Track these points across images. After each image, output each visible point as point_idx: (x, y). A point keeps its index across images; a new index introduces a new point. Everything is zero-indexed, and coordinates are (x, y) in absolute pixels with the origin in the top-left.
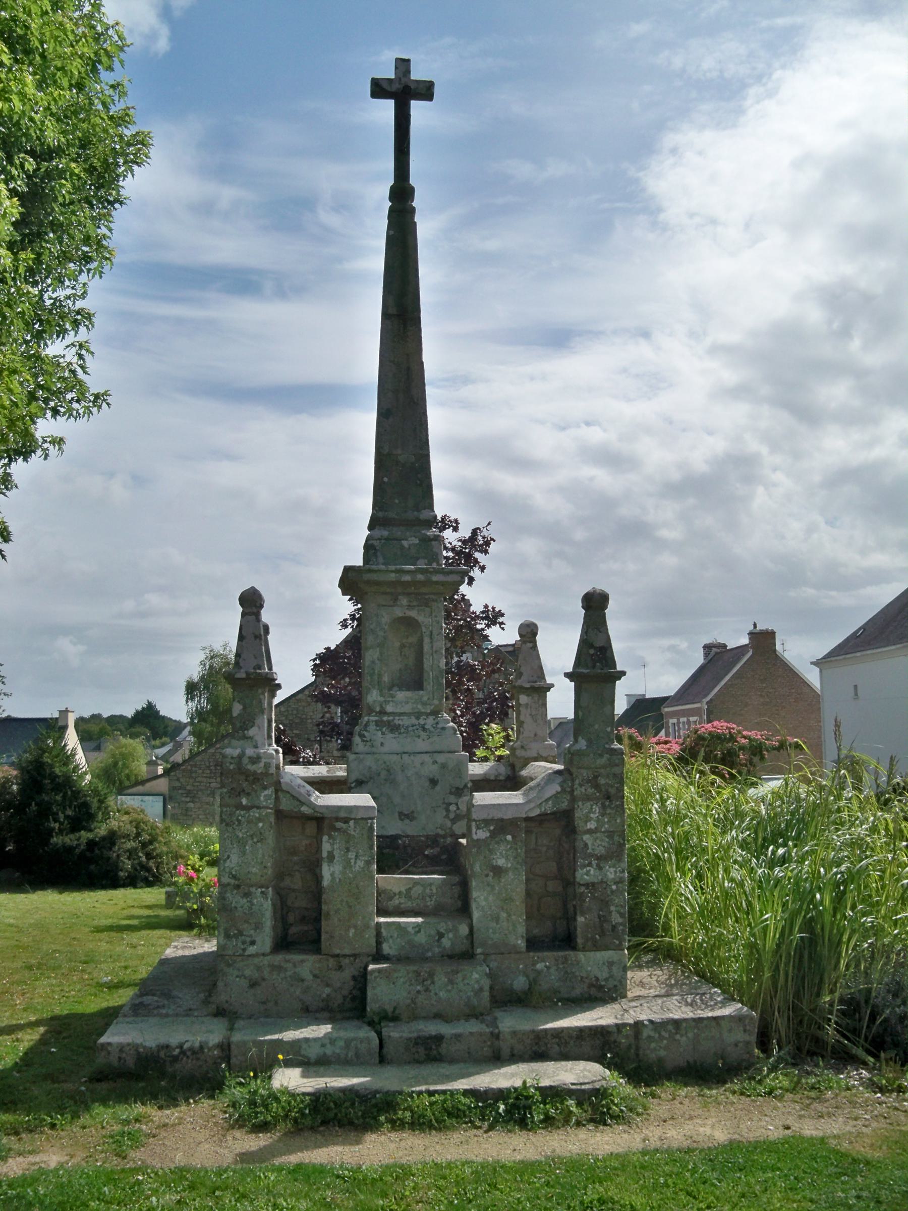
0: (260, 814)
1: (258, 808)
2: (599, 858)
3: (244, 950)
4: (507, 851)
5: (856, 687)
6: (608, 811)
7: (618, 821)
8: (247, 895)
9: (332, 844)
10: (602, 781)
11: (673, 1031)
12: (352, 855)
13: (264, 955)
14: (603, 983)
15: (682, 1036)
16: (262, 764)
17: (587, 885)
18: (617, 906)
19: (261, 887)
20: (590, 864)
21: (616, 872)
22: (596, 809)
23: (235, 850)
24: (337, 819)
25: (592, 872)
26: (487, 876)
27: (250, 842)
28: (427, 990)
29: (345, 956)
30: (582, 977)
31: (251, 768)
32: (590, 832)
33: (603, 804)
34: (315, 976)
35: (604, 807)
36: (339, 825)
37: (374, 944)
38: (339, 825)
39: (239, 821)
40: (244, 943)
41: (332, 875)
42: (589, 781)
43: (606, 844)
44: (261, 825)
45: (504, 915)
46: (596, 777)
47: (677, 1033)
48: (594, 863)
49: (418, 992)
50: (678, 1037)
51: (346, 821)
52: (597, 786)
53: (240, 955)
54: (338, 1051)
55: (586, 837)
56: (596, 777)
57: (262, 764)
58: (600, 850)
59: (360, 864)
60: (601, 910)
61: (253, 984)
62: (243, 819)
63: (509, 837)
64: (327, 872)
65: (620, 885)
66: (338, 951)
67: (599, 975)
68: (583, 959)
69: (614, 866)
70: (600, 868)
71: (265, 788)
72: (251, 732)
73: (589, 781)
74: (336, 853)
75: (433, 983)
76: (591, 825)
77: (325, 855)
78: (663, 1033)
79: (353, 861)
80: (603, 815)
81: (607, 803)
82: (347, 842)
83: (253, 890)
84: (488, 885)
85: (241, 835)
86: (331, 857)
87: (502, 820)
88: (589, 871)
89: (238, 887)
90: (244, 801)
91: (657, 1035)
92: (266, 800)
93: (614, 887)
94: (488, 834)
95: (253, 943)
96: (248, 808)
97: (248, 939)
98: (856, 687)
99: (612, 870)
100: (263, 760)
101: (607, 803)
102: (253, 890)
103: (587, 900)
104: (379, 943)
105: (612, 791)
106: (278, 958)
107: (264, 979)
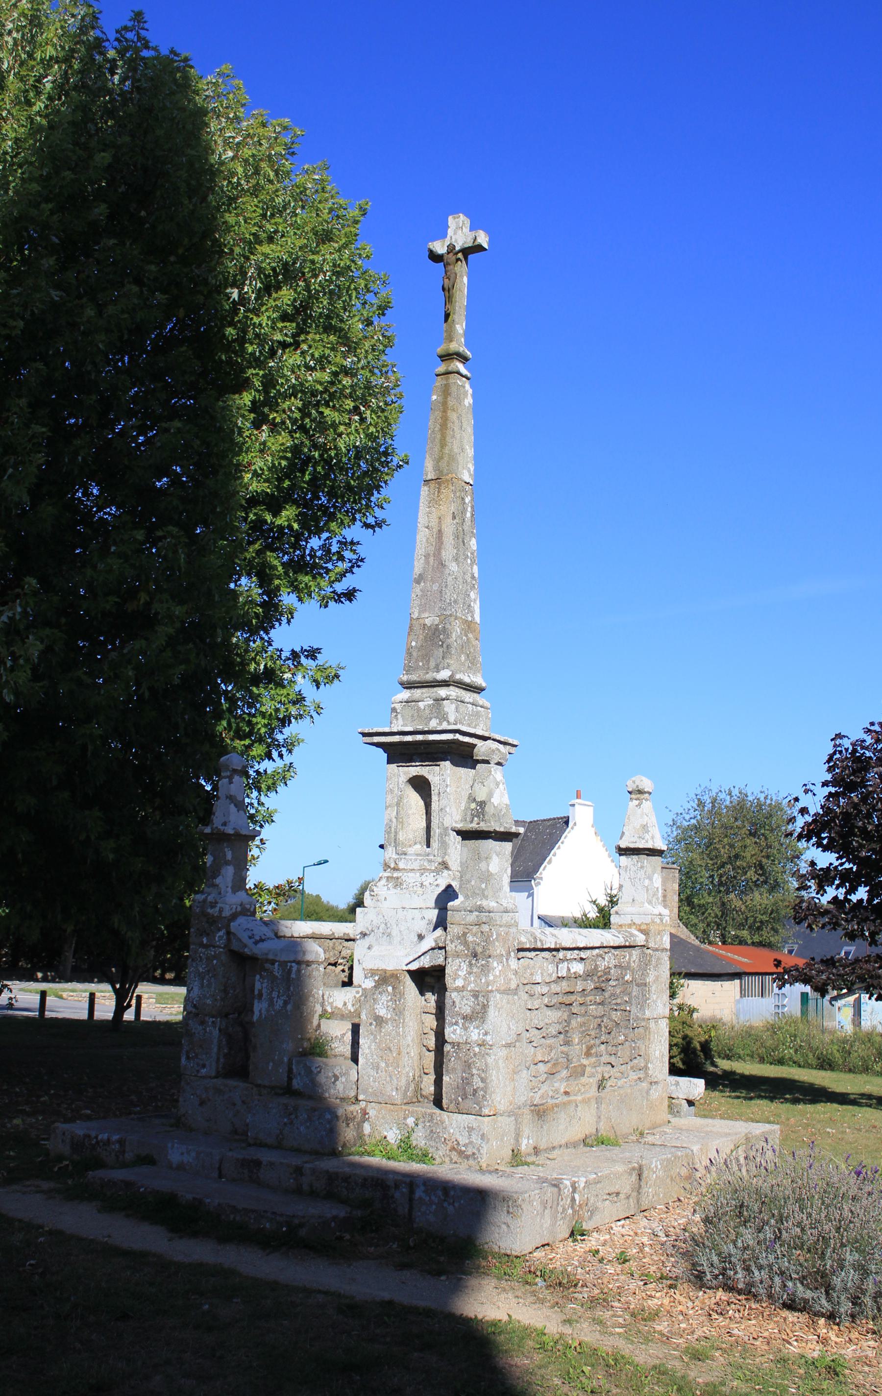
0: (215, 952)
1: (214, 947)
2: (465, 1018)
3: (198, 1071)
4: (388, 1001)
5: (326, 861)
6: (475, 970)
7: (483, 981)
8: (202, 1023)
9: (262, 983)
10: (470, 938)
11: (442, 1198)
12: (275, 994)
13: (210, 1077)
14: (463, 1149)
15: (449, 1204)
16: (217, 909)
17: (453, 1044)
18: (478, 1070)
19: (213, 1017)
20: (456, 1023)
21: (479, 1034)
22: (464, 966)
23: (196, 983)
24: (267, 961)
25: (458, 1031)
26: (371, 1024)
27: (207, 977)
28: (291, 1123)
29: (265, 1087)
30: (445, 1139)
31: (210, 911)
32: (458, 990)
33: (470, 962)
34: (243, 1102)
35: (471, 964)
36: (268, 966)
37: (286, 1079)
38: (268, 966)
39: (201, 957)
40: (198, 1065)
41: (260, 1011)
42: (459, 938)
43: (472, 1004)
44: (215, 962)
45: (383, 1065)
46: (465, 934)
47: (445, 1200)
48: (461, 1021)
49: (285, 1124)
50: (446, 1204)
51: (273, 962)
52: (466, 943)
53: (195, 1076)
54: (191, 1160)
55: (454, 995)
56: (465, 934)
57: (217, 909)
58: (467, 1010)
59: (281, 1002)
60: (464, 1071)
61: (202, 1103)
62: (204, 957)
63: (390, 989)
64: (259, 1008)
65: (483, 1048)
66: (259, 1082)
67: (460, 1139)
68: (447, 1120)
69: (477, 1028)
70: (466, 1029)
71: (219, 930)
72: (218, 881)
73: (459, 938)
74: (264, 991)
75: (296, 1117)
76: (459, 983)
77: (256, 992)
78: (433, 1198)
79: (275, 1000)
80: (470, 973)
81: (474, 962)
82: (272, 982)
83: (207, 1019)
84: (372, 1034)
85: (201, 970)
86: (260, 995)
87: (385, 971)
88: (455, 1030)
89: (197, 1015)
90: (205, 940)
91: (428, 1198)
92: (219, 941)
93: (477, 1049)
94: (374, 984)
95: (204, 1066)
96: (206, 947)
97: (201, 1062)
98: (326, 861)
99: (476, 1031)
100: (219, 905)
101: (474, 962)
102: (207, 1019)
103: (453, 1059)
104: (290, 1079)
105: (479, 950)
106: (219, 1082)
107: (209, 1100)
